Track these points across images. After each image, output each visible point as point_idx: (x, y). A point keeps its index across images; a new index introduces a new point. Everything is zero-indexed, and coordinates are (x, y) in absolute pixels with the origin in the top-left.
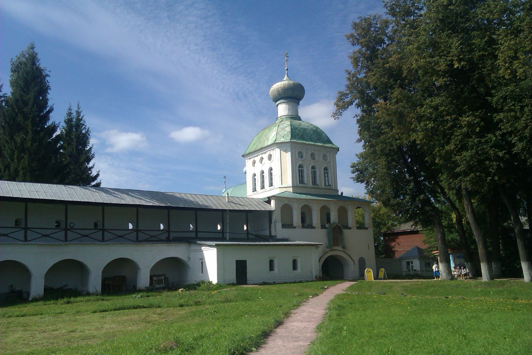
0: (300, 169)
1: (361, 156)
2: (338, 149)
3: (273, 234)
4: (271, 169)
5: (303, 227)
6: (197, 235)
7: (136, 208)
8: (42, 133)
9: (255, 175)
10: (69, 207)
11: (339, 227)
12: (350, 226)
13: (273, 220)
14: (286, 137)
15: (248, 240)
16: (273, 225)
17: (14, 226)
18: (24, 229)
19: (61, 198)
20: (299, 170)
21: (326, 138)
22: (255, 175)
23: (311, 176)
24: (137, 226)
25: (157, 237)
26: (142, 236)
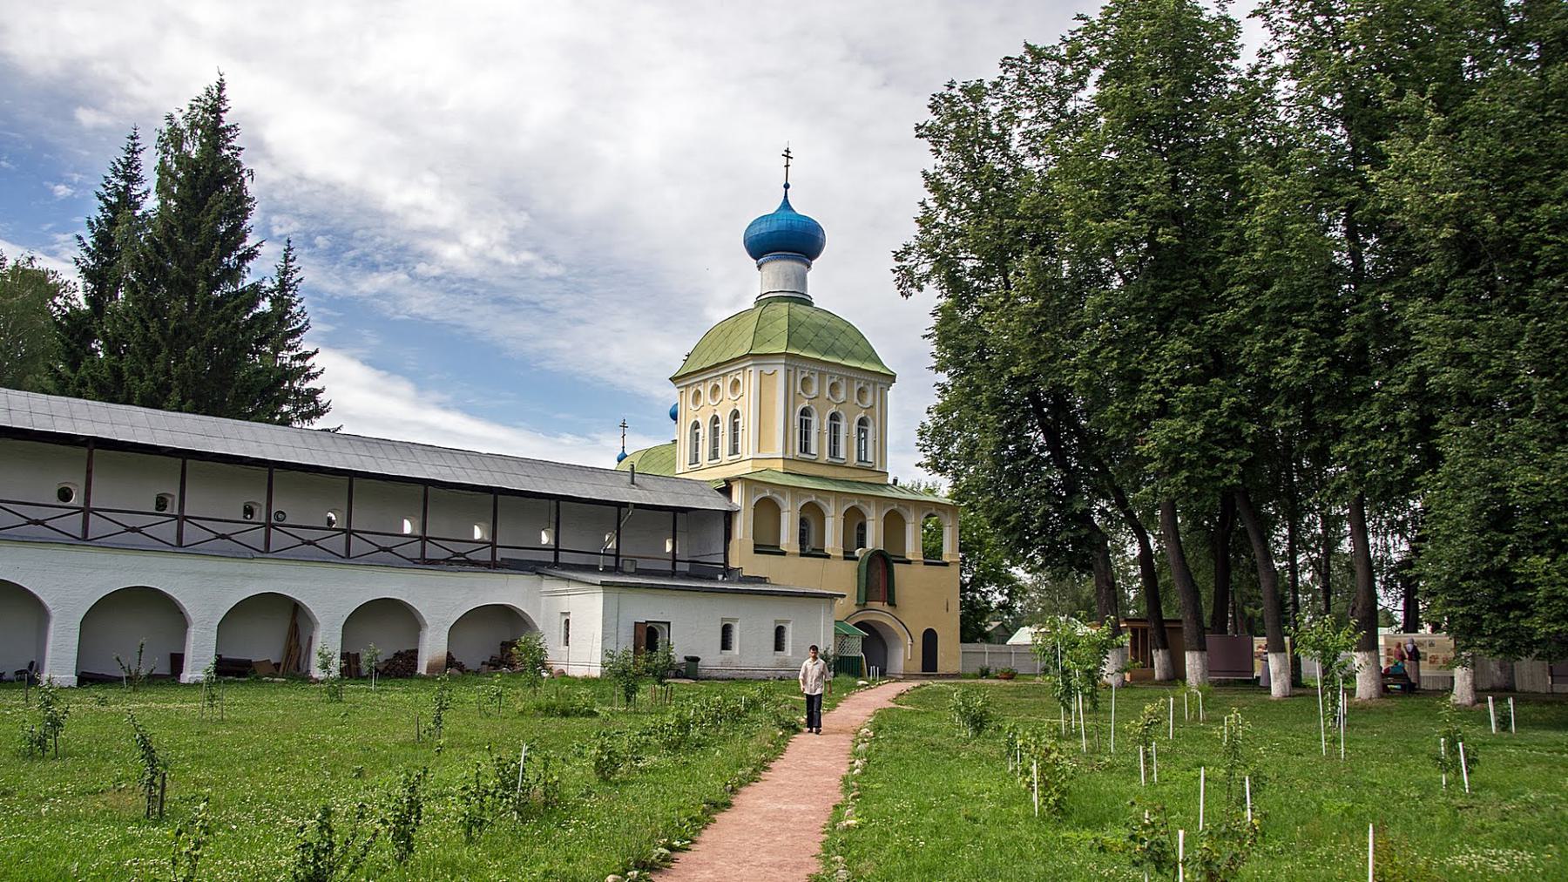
0: (804, 418)
2: (891, 378)
4: (736, 414)
7: (180, 460)
8: (1041, 439)
9: (696, 425)
10: (277, 473)
12: (783, 548)
15: (673, 574)
17: (326, 526)
18: (176, 517)
20: (801, 420)
22: (696, 425)
23: (827, 437)
24: (424, 529)
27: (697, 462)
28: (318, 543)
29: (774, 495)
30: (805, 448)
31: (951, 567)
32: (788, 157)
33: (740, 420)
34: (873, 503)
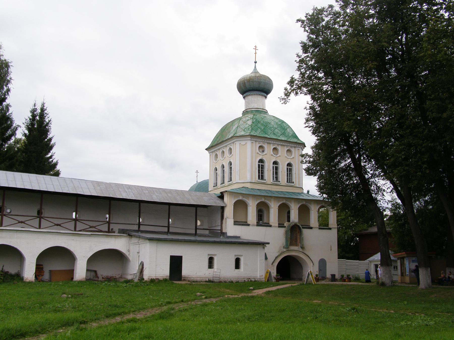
3: (224, 231)
5: (258, 225)
6: (139, 227)
12: (311, 226)
13: (225, 216)
14: (247, 130)
19: (81, 192)
21: (291, 133)
22: (216, 169)
25: (96, 227)
28: (26, 222)
29: (307, 203)
30: (261, 176)
32: (256, 49)
33: (232, 166)
34: (266, 144)
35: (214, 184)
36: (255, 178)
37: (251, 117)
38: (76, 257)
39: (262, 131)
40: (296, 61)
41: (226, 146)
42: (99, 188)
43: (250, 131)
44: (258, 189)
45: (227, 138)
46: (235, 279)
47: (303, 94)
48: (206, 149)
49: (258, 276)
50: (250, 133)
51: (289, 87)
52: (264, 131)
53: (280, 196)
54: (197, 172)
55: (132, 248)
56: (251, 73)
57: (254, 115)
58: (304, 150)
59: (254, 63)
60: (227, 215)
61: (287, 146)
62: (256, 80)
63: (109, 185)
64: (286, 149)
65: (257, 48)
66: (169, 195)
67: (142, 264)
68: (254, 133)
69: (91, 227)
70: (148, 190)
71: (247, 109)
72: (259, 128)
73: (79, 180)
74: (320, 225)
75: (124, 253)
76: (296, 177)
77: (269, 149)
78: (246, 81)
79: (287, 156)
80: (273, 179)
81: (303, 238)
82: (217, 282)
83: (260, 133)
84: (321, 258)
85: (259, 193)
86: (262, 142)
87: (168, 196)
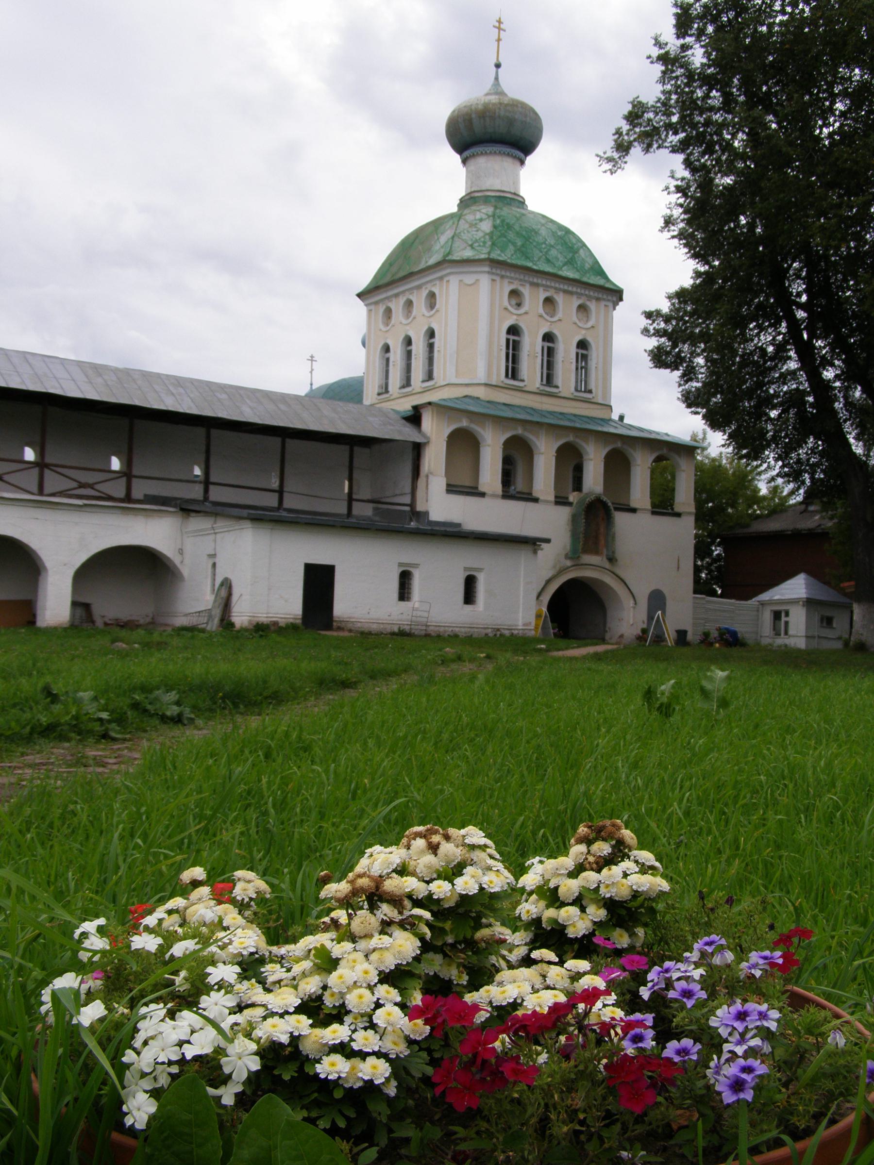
0: (512, 337)
1: (682, 295)
3: (420, 508)
4: (431, 334)
5: (507, 495)
6: (206, 491)
11: (604, 504)
12: (634, 504)
14: (479, 246)
16: (421, 482)
20: (508, 341)
21: (590, 261)
22: (387, 349)
25: (97, 487)
26: (53, 481)
27: (387, 391)
30: (513, 372)
31: (684, 518)
32: (499, 29)
33: (437, 341)
34: (528, 286)
35: (380, 387)
36: (498, 375)
37: (490, 213)
38: (43, 564)
39: (519, 250)
40: (649, 57)
41: (419, 287)
42: (100, 380)
43: (488, 250)
44: (504, 404)
45: (422, 265)
46: (463, 630)
47: (667, 151)
48: (359, 295)
49: (520, 623)
50: (489, 253)
51: (625, 127)
52: (522, 252)
53: (562, 423)
54: (312, 359)
55: (189, 544)
56: (487, 94)
57: (496, 207)
58: (617, 307)
59: (494, 69)
60: (429, 466)
61: (579, 295)
62: (502, 113)
63: (125, 375)
64: (576, 302)
65: (502, 26)
66: (283, 407)
67: (227, 584)
68: (499, 255)
69: (82, 486)
70: (226, 393)
71: (475, 192)
72: (510, 241)
73: (46, 359)
74: (654, 505)
75: (168, 558)
76: (597, 379)
77: (533, 299)
78: (473, 116)
79: (578, 322)
80: (542, 380)
81: (614, 534)
82: (420, 636)
83: (512, 255)
84: (654, 588)
85: (508, 414)
86: (516, 279)
87: (280, 409)
